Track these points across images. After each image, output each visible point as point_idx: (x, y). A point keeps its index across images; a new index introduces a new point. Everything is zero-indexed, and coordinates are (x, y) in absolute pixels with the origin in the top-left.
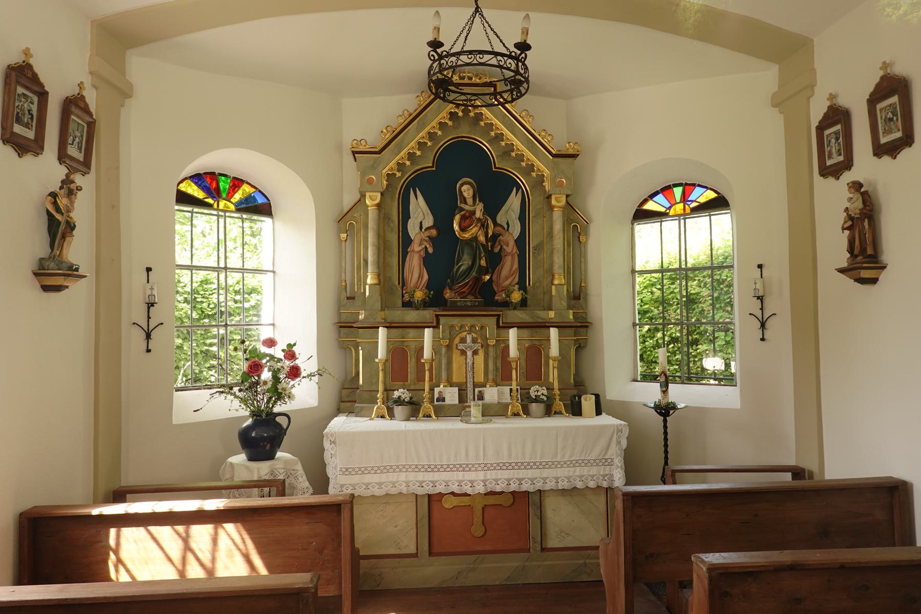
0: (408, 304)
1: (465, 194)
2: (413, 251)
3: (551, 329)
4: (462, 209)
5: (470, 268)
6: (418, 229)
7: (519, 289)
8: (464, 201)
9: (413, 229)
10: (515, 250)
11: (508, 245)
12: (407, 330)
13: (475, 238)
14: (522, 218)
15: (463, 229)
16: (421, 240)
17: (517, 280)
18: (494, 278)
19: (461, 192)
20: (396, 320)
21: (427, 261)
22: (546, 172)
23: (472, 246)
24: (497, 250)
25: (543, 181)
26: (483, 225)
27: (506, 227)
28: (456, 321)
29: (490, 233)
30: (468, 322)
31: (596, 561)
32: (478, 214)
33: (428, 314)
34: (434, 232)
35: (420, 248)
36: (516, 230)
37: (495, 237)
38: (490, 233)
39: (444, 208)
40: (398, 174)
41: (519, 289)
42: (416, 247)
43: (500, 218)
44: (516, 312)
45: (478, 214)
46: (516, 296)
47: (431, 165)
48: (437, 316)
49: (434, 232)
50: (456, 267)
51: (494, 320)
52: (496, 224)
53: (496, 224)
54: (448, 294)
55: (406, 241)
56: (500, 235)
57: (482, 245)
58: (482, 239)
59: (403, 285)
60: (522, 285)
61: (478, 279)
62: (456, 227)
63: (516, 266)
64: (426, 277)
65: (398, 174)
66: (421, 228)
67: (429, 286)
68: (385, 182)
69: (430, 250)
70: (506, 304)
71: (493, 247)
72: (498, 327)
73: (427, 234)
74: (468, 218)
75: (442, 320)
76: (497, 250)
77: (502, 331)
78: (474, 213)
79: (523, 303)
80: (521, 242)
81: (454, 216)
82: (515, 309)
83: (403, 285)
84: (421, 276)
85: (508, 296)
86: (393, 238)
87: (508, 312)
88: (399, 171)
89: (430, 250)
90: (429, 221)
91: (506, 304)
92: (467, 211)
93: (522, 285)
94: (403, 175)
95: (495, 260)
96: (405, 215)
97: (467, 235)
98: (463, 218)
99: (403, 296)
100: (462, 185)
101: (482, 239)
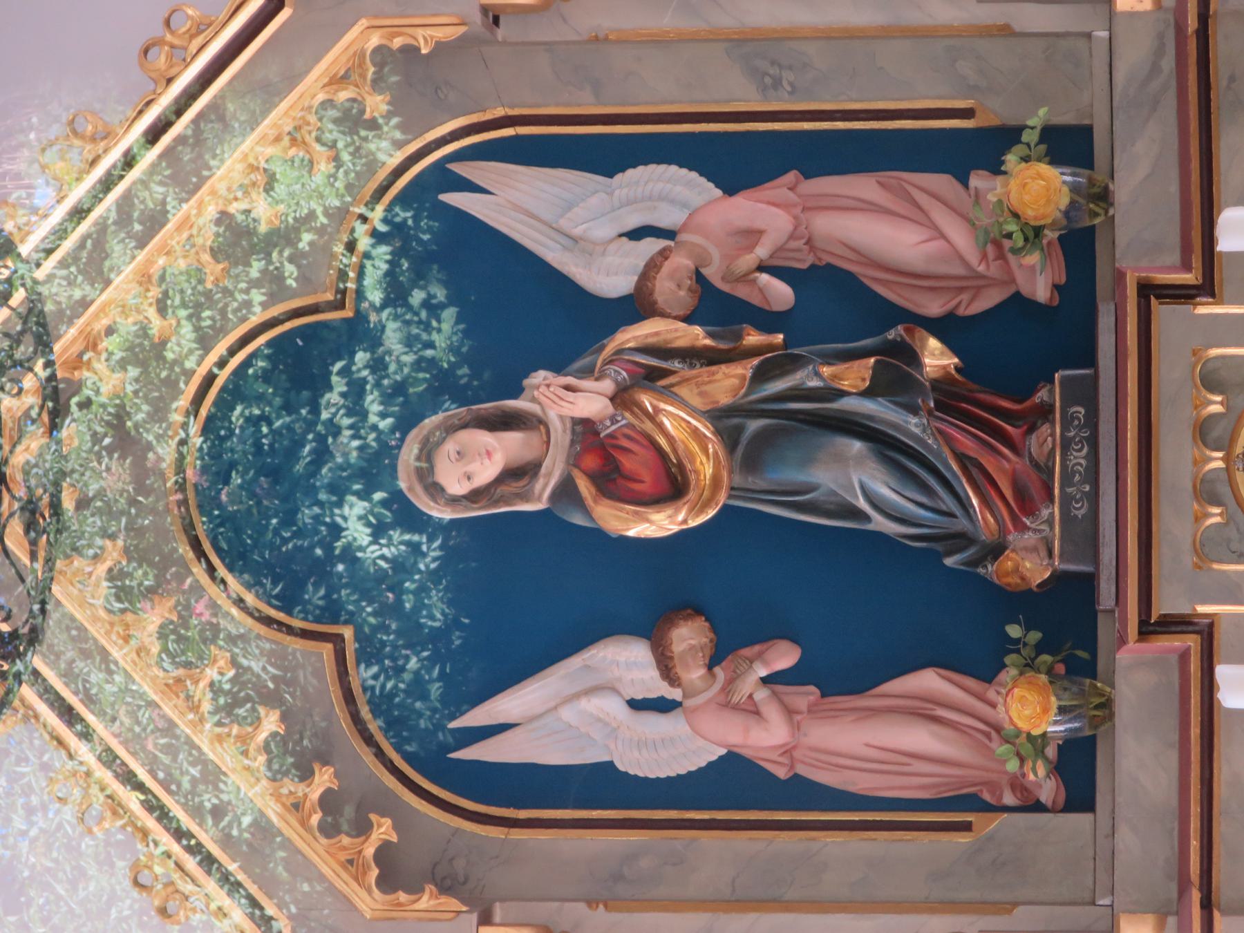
0: (1080, 771)
1: (486, 472)
2: (788, 751)
3: (1226, 243)
4: (566, 491)
5: (886, 445)
6: (654, 723)
7: (996, 168)
8: (519, 474)
9: (668, 749)
10: (780, 188)
11: (752, 235)
12: (1221, 790)
13: (725, 420)
14: (603, 153)
15: (673, 486)
16: (727, 704)
17: (942, 182)
18: (934, 307)
19: (475, 496)
20: (1165, 850)
21: (840, 673)
22: (362, 37)
23: (764, 439)
24: (780, 293)
25: (410, 51)
26: (651, 377)
27: (651, 246)
28: (1175, 527)
29: (697, 335)
30: (1177, 458)
31: (1063, 703)
32: (591, 401)
33: (1137, 673)
34: (688, 637)
35: (772, 712)
36: (670, 191)
37: (715, 306)
38: (697, 335)
39: (533, 588)
40: (383, 830)
41: (996, 168)
42: (766, 738)
43: (610, 276)
44: (1123, 191)
45: (591, 401)
46: (1038, 187)
47: (327, 649)
48: (1150, 628)
49: (688, 637)
50: (880, 523)
51: (1163, 312)
52: (636, 306)
53: (636, 306)
54: (1029, 564)
55: (732, 789)
56: (699, 277)
57: (761, 375)
58: (728, 383)
59: (973, 803)
60: (974, 150)
61: (948, 399)
62: (659, 524)
63: (864, 186)
64: (929, 681)
65: (383, 830)
66: (662, 706)
67: (983, 667)
68: (426, 901)
69: (785, 657)
70: (1079, 245)
71: (766, 320)
72: (1208, 288)
73: (694, 674)
74: (606, 460)
75: (1167, 603)
76: (780, 293)
77: (1224, 274)
78: (585, 429)
79: (1069, 145)
80: (735, 157)
81: (598, 534)
82: (1103, 197)
83: (973, 803)
84: (924, 711)
85: (1034, 234)
86: (719, 854)
87: (1123, 235)
88: (362, 829)
89: (785, 657)
90: (627, 661)
91: (1079, 245)
92: (575, 461)
93: (974, 150)
94: (389, 807)
95: (840, 303)
96: (596, 789)
97: (705, 466)
98: (612, 480)
99: (1037, 807)
100: (435, 490)
101: (728, 383)
